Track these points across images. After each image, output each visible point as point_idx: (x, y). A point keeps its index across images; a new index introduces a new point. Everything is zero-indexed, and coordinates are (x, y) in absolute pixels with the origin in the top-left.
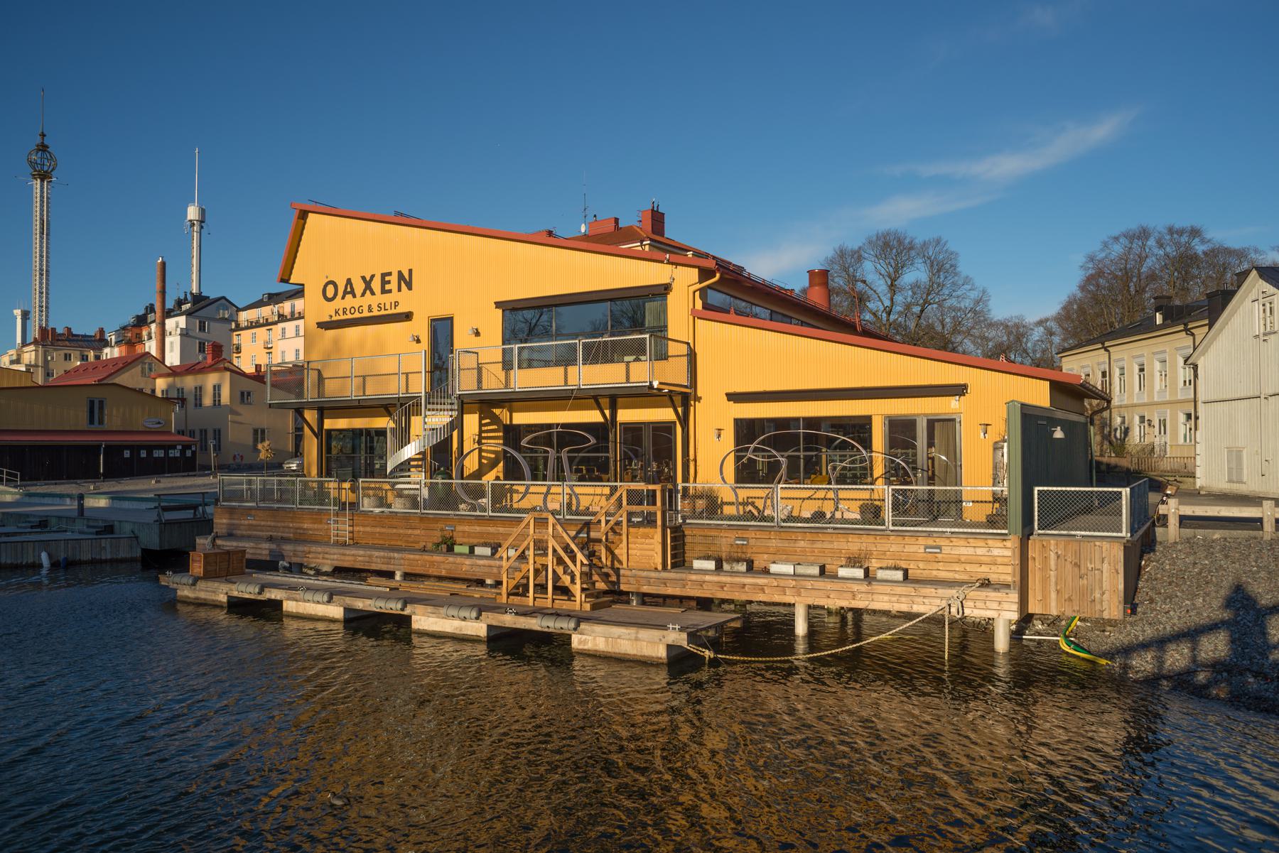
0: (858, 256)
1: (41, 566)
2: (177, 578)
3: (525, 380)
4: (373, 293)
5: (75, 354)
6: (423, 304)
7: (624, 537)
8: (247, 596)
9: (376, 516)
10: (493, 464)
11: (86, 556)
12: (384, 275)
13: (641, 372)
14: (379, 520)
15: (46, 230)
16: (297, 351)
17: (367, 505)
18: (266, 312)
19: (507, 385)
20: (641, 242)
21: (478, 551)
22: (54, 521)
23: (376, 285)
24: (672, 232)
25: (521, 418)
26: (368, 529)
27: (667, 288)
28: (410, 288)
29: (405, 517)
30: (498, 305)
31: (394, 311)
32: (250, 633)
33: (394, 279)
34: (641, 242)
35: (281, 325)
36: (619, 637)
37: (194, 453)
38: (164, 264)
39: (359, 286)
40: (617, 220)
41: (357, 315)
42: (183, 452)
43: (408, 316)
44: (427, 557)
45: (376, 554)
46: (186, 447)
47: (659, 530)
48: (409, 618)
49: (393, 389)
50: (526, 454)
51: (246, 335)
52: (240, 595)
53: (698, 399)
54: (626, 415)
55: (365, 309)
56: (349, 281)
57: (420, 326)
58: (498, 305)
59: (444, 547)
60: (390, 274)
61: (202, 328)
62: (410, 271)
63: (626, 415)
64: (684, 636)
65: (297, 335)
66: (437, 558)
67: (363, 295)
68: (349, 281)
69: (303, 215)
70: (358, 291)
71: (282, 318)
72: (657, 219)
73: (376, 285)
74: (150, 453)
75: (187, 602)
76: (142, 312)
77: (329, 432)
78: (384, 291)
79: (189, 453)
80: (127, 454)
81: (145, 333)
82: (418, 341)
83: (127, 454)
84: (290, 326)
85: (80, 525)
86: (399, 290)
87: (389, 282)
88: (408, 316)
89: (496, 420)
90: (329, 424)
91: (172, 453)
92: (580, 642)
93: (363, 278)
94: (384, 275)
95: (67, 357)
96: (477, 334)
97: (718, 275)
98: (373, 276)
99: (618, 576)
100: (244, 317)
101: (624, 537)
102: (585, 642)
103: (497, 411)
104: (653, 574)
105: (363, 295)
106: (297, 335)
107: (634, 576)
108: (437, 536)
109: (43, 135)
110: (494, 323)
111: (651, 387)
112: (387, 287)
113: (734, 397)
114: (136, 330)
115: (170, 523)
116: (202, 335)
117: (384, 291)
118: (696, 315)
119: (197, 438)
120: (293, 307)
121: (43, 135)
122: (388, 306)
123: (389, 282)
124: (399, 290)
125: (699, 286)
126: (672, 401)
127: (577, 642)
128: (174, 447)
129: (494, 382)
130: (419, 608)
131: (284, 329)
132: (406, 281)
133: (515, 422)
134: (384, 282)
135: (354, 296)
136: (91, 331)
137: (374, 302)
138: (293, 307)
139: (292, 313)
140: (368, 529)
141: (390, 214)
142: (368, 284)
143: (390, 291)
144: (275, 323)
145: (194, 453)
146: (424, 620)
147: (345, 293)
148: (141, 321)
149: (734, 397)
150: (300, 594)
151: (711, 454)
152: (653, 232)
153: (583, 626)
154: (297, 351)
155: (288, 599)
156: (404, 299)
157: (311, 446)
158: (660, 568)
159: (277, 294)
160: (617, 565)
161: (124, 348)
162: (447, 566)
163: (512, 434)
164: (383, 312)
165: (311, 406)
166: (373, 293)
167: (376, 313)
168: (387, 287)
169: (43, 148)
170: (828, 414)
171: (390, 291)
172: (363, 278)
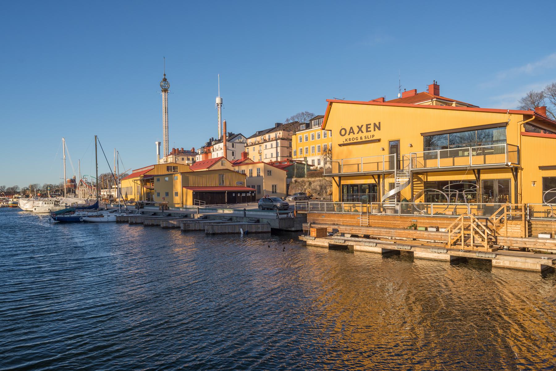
0: (541, 96)
1: (240, 233)
2: (307, 237)
3: (431, 164)
4: (362, 132)
5: (185, 158)
6: (386, 136)
7: (505, 224)
8: (338, 244)
9: (379, 216)
10: (419, 196)
11: (254, 231)
12: (367, 125)
13: (493, 160)
14: (382, 218)
15: (167, 112)
16: (272, 154)
17: (374, 212)
18: (259, 139)
19: (425, 166)
20: (432, 99)
21: (429, 229)
22: (234, 218)
23: (364, 129)
24: (443, 94)
25: (431, 179)
26: (376, 221)
27: (507, 124)
28: (379, 129)
29: (393, 217)
30: (422, 134)
31: (372, 139)
32: (342, 256)
33: (372, 126)
34: (432, 99)
35: (265, 144)
36: (517, 261)
37: (255, 194)
38: (226, 122)
39: (356, 130)
40: (416, 90)
41: (355, 141)
42: (251, 193)
43: (379, 140)
44: (407, 231)
45: (383, 230)
46: (252, 192)
47: (523, 222)
48: (413, 252)
49: (372, 168)
50: (436, 192)
51: (251, 148)
52: (335, 243)
53: (522, 169)
54: (483, 177)
55: (359, 138)
56: (351, 128)
57: (385, 144)
58: (422, 134)
59: (413, 228)
60: (370, 124)
61: (233, 146)
62: (379, 123)
63: (483, 177)
64: (550, 261)
65: (272, 147)
66: (411, 232)
67: (358, 133)
68: (351, 128)
69: (331, 104)
70: (356, 131)
71: (265, 141)
72: (436, 88)
73: (364, 129)
74: (241, 194)
75: (311, 245)
76: (209, 141)
77: (343, 185)
78: (367, 131)
79: (253, 194)
80: (234, 195)
81: (211, 149)
82: (383, 150)
83: (234, 195)
84: (268, 144)
85: (245, 220)
86: (375, 130)
87: (370, 128)
88: (379, 140)
89: (420, 179)
90: (343, 182)
91: (249, 195)
92: (496, 263)
93: (358, 127)
94: (367, 125)
95: (183, 159)
96: (411, 146)
97: (534, 117)
98: (362, 126)
99: (496, 239)
100: (249, 141)
101: (505, 224)
102: (499, 263)
103: (420, 176)
104: (521, 239)
105: (358, 133)
106: (272, 147)
107: (509, 240)
108: (409, 224)
109: (165, 75)
110: (420, 142)
111: (507, 165)
112: (369, 130)
113: (542, 168)
114: (208, 148)
115: (282, 219)
116: (233, 149)
117: (367, 131)
118: (522, 134)
119: (256, 189)
120: (269, 136)
121: (165, 75)
122: (369, 137)
123: (370, 128)
124: (375, 130)
125: (523, 122)
126: (474, 172)
127: (494, 262)
128: (248, 192)
129: (420, 165)
130: (417, 249)
131: (272, 144)
132: (378, 127)
133: (429, 180)
134: (367, 128)
135: (354, 134)
136: (190, 149)
137: (364, 135)
138: (269, 136)
139: (269, 139)
140: (376, 221)
141: (367, 100)
142: (360, 129)
143: (370, 131)
144: (263, 143)
145: (255, 194)
146: (418, 253)
147: (350, 132)
148: (209, 144)
149: (542, 168)
150: (361, 243)
151: (530, 191)
152: (435, 94)
153: (498, 257)
154: (272, 154)
155: (356, 245)
156: (377, 135)
157: (335, 189)
158: (524, 236)
159: (262, 131)
160: (497, 235)
161: (204, 155)
162: (417, 235)
163: (428, 185)
164: (367, 139)
165: (336, 176)
166: (362, 132)
167: (364, 140)
168: (369, 130)
169: (165, 80)
170: (498, 174)
171: (370, 131)
172: (358, 127)
